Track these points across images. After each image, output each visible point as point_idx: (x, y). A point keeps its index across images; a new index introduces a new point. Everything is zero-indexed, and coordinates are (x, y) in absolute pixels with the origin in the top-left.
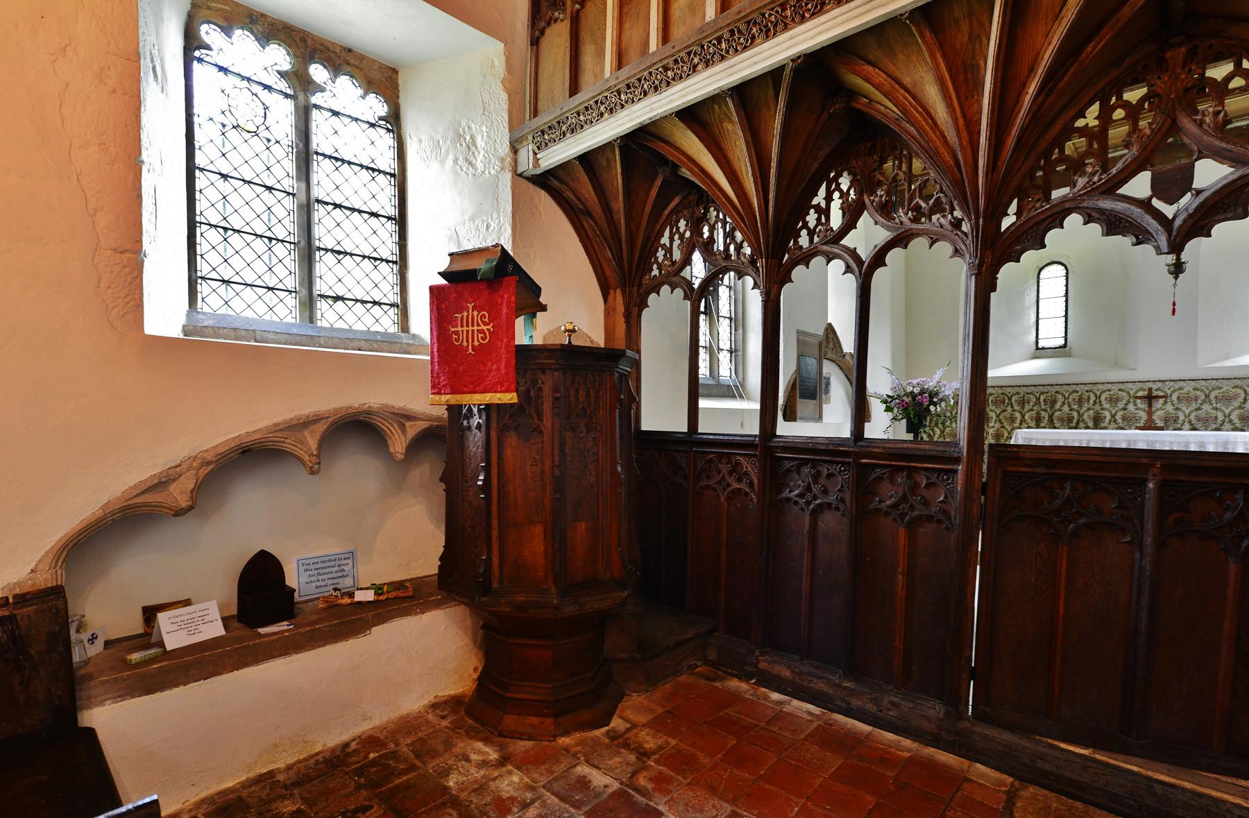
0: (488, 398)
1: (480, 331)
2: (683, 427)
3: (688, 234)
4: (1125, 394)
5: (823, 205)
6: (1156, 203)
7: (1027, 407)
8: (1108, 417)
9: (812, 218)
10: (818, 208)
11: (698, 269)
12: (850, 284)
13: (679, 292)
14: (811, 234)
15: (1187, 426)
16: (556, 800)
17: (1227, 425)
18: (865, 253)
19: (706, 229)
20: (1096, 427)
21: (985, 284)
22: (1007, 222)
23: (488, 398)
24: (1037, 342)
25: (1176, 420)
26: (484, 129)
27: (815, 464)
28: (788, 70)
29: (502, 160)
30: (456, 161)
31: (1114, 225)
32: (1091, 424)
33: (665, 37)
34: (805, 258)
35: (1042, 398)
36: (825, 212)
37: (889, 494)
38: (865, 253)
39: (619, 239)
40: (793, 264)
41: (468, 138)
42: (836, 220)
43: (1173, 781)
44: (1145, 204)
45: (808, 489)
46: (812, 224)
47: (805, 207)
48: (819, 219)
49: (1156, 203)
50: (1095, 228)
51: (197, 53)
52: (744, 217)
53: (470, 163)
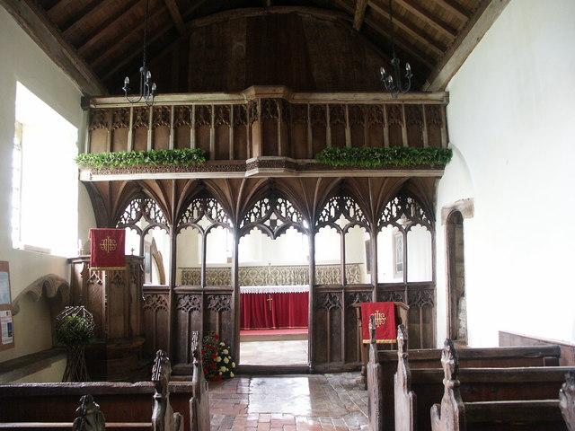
3: (139, 210)
12: (200, 237)
13: (350, 229)
16: (350, 375)
18: (205, 228)
20: (248, 285)
21: (237, 243)
27: (190, 295)
28: (335, 182)
31: (264, 231)
33: (153, 147)
34: (186, 227)
36: (191, 212)
37: (214, 302)
38: (205, 228)
39: (112, 208)
42: (196, 216)
43: (191, 408)
44: (269, 227)
45: (188, 304)
46: (187, 216)
51: (159, 221)
52: (166, 210)
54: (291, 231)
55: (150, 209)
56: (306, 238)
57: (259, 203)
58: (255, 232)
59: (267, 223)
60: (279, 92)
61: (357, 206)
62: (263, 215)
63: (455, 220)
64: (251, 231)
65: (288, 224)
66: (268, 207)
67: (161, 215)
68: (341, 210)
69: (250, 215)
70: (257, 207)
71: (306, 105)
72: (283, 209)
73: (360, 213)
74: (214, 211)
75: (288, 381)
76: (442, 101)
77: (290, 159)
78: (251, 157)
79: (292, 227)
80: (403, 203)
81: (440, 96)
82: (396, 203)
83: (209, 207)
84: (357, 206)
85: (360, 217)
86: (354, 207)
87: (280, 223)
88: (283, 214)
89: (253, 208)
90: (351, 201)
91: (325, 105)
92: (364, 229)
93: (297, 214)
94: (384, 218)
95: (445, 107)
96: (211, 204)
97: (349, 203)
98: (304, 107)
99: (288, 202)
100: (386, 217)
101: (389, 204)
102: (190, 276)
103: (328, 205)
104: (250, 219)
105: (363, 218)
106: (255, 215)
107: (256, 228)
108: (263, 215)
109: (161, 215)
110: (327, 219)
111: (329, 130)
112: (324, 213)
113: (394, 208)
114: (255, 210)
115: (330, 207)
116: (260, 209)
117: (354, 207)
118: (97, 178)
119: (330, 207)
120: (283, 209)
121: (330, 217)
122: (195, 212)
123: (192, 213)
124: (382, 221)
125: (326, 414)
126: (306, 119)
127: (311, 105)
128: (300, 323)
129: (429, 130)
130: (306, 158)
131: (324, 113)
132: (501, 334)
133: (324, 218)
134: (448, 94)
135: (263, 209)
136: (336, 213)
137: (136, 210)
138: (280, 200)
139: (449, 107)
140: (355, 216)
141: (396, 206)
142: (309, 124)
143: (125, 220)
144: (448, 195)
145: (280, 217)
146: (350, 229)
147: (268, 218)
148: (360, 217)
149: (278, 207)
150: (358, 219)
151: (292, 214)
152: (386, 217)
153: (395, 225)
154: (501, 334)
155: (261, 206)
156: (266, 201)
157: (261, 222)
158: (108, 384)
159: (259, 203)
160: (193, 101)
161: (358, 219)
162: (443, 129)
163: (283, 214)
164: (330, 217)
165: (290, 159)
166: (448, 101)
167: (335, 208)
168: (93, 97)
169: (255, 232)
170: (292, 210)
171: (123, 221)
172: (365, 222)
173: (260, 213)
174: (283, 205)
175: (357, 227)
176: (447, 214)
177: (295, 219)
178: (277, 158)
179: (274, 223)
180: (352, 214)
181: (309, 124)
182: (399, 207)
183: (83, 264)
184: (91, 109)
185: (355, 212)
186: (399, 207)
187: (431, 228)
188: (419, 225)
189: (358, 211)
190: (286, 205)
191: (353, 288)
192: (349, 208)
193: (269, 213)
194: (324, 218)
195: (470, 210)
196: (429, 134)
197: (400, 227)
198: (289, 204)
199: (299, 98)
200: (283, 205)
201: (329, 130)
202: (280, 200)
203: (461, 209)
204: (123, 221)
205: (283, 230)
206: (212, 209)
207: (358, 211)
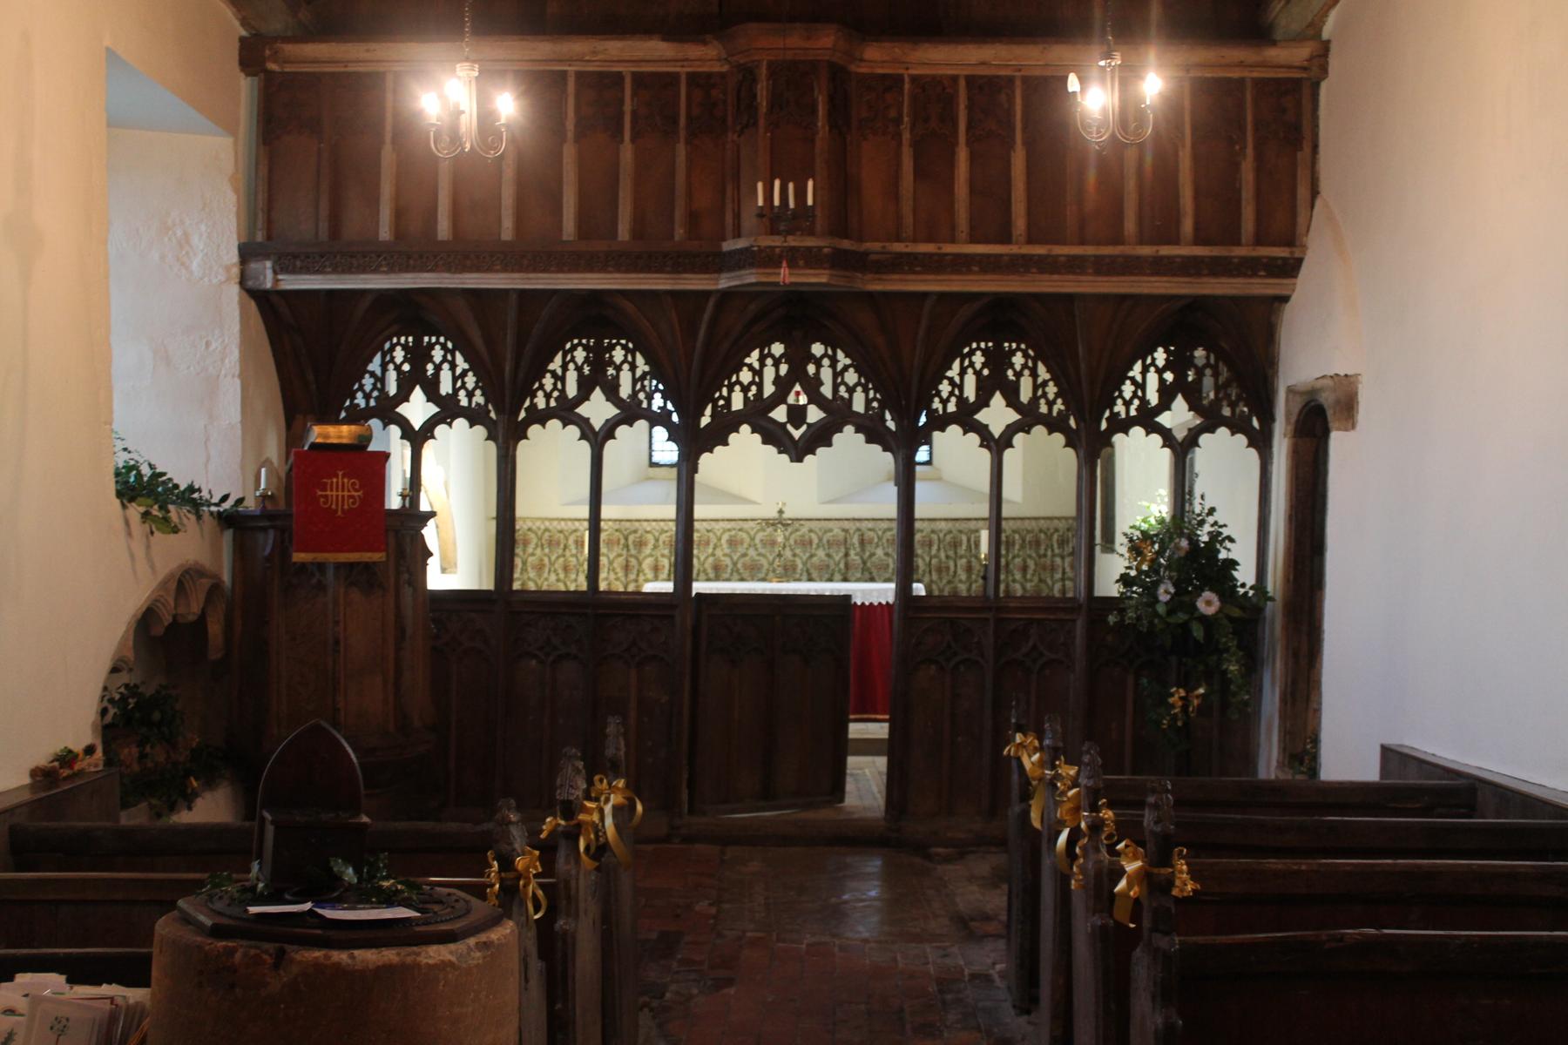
0: (344, 557)
1: (350, 497)
2: (582, 584)
4: (744, 535)
5: (559, 372)
6: (789, 427)
7: (647, 550)
8: (535, 541)
9: (548, 382)
10: (554, 373)
11: (417, 409)
14: (548, 396)
15: (805, 576)
17: (736, 576)
19: (430, 368)
22: (705, 420)
23: (344, 557)
24: (651, 456)
25: (794, 568)
26: (203, 228)
29: (228, 269)
30: (163, 257)
32: (712, 575)
34: (541, 418)
35: (631, 538)
40: (529, 422)
41: (179, 233)
46: (548, 388)
47: (541, 372)
48: (555, 384)
49: (789, 427)
50: (757, 437)
51: (464, 402)
53: (183, 264)
54: (848, 439)
55: (438, 368)
56: (882, 461)
57: (756, 354)
58: (745, 439)
59: (780, 414)
60: (825, 42)
61: (1041, 369)
62: (769, 389)
63: (1317, 422)
64: (733, 437)
65: (838, 415)
66: (784, 369)
67: (470, 386)
68: (995, 382)
69: (731, 390)
70: (750, 367)
71: (899, 79)
72: (826, 374)
73: (1052, 390)
74: (625, 379)
75: (892, 492)
76: (1305, 69)
77: (846, 244)
78: (738, 234)
79: (849, 429)
80: (1178, 363)
81: (1300, 54)
82: (1161, 362)
83: (611, 362)
84: (1041, 369)
85: (1050, 404)
86: (1034, 375)
87: (814, 414)
88: (827, 390)
89: (738, 370)
90: (1026, 355)
91: (955, 79)
92: (1059, 438)
93: (866, 391)
94: (1119, 407)
95: (1315, 87)
96: (618, 355)
97: (1018, 360)
98: (895, 81)
99: (840, 355)
100: (1127, 404)
101: (1138, 367)
102: (550, 572)
103: (956, 365)
104: (728, 400)
105: (1059, 406)
106: (745, 389)
107: (745, 429)
108: (769, 389)
109: (470, 386)
110: (951, 407)
111: (962, 155)
112: (945, 388)
113: (1152, 378)
114: (746, 376)
115: (963, 373)
116: (758, 373)
117: (1034, 375)
118: (291, 283)
119: (963, 373)
120: (826, 374)
121: (961, 401)
122: (572, 376)
123: (563, 379)
124: (1114, 415)
125: (918, 938)
126: (898, 121)
127: (914, 79)
128: (1382, 776)
129: (1259, 157)
130: (899, 240)
131: (949, 102)
132: (1386, 751)
133: (945, 402)
134: (1325, 48)
135: (769, 373)
136: (978, 389)
137: (398, 368)
138: (817, 349)
139: (1324, 86)
140: (1035, 400)
141: (1160, 372)
142: (906, 136)
143: (367, 397)
144: (1305, 360)
145: (816, 398)
146: (1019, 439)
147: (779, 398)
148: (1050, 404)
149: (811, 369)
150: (1044, 409)
151: (851, 390)
152: (1127, 404)
153: (1152, 427)
154: (1386, 751)
155: (763, 365)
156: (778, 349)
157: (757, 415)
158: (35, 951)
159: (756, 354)
160: (570, 61)
161: (1044, 409)
162: (1303, 155)
163: (827, 390)
164: (961, 401)
165: (846, 244)
166: (1324, 71)
167: (978, 373)
168: (275, 39)
169: (745, 439)
170: (851, 377)
171: (360, 400)
172: (1063, 417)
173: (760, 386)
174: (826, 362)
175: (1039, 430)
176: (1297, 404)
177: (859, 405)
178: (810, 242)
179: (797, 415)
180: (1025, 394)
181: (906, 136)
182: (1169, 376)
183: (271, 533)
184: (270, 74)
185: (1035, 387)
186: (1169, 376)
187: (1261, 442)
188: (1223, 431)
189: (1045, 383)
190: (834, 362)
191: (1017, 610)
192: (1018, 375)
193: (783, 386)
194: (945, 402)
195: (1348, 407)
196: (1260, 169)
197: (1167, 436)
198: (843, 360)
199: (877, 57)
200: (826, 362)
201: (962, 155)
202: (817, 349)
203: (1327, 399)
204: (360, 400)
205: (821, 437)
206: (618, 368)
207: (1045, 383)
